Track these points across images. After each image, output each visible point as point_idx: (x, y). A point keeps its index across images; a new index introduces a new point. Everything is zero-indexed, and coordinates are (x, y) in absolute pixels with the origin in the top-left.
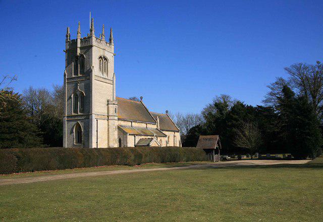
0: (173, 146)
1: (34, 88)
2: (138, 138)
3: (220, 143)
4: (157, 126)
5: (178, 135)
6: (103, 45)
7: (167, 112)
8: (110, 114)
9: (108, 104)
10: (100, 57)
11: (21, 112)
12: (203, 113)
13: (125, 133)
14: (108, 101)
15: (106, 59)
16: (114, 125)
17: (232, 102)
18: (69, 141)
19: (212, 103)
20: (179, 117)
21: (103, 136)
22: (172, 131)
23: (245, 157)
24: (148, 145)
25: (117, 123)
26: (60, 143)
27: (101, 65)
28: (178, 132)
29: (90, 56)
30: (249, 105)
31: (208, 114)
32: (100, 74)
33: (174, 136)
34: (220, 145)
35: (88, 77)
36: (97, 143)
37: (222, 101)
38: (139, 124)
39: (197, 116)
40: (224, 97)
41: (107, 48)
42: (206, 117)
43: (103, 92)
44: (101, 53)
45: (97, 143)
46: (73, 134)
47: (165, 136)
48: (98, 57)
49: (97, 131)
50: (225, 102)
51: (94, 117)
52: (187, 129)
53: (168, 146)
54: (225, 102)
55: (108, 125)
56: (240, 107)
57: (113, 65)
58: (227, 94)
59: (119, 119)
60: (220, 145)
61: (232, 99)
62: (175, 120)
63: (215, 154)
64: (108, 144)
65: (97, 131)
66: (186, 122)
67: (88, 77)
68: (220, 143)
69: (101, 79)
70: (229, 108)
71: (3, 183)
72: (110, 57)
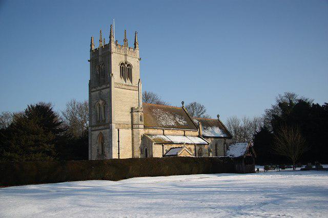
1: (81, 102)
7: (218, 116)
8: (135, 122)
9: (132, 112)
13: (150, 142)
14: (132, 109)
16: (139, 134)
18: (93, 155)
19: (275, 103)
21: (123, 146)
23: (261, 169)
24: (177, 155)
25: (142, 132)
26: (86, 157)
27: (124, 72)
30: (315, 103)
32: (122, 81)
35: (108, 86)
36: (119, 153)
43: (124, 100)
45: (119, 153)
49: (119, 141)
51: (114, 125)
55: (133, 134)
57: (139, 70)
58: (291, 92)
64: (133, 154)
65: (119, 141)
67: (108, 86)
69: (124, 87)
71: (96, 194)
72: (133, 61)
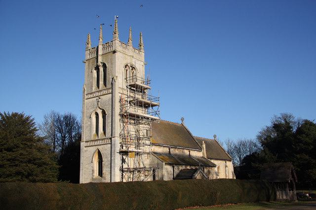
0: (225, 178)
2: (181, 168)
3: (295, 174)
4: (203, 154)
5: (230, 165)
6: (130, 51)
10: (126, 66)
11: (31, 140)
12: (259, 138)
15: (133, 68)
17: (295, 123)
19: (270, 124)
20: (229, 145)
22: (222, 160)
28: (230, 161)
29: (113, 63)
31: (265, 139)
33: (226, 166)
34: (295, 176)
37: (283, 122)
38: (179, 150)
39: (251, 143)
40: (286, 117)
41: (135, 55)
42: (263, 144)
44: (129, 61)
46: (92, 165)
47: (214, 166)
48: (123, 65)
50: (286, 122)
52: (240, 158)
53: (218, 178)
54: (286, 122)
56: (308, 126)
59: (153, 144)
60: (295, 176)
61: (296, 119)
62: (225, 147)
63: (290, 190)
66: (238, 150)
68: (295, 174)
70: (259, 145)
